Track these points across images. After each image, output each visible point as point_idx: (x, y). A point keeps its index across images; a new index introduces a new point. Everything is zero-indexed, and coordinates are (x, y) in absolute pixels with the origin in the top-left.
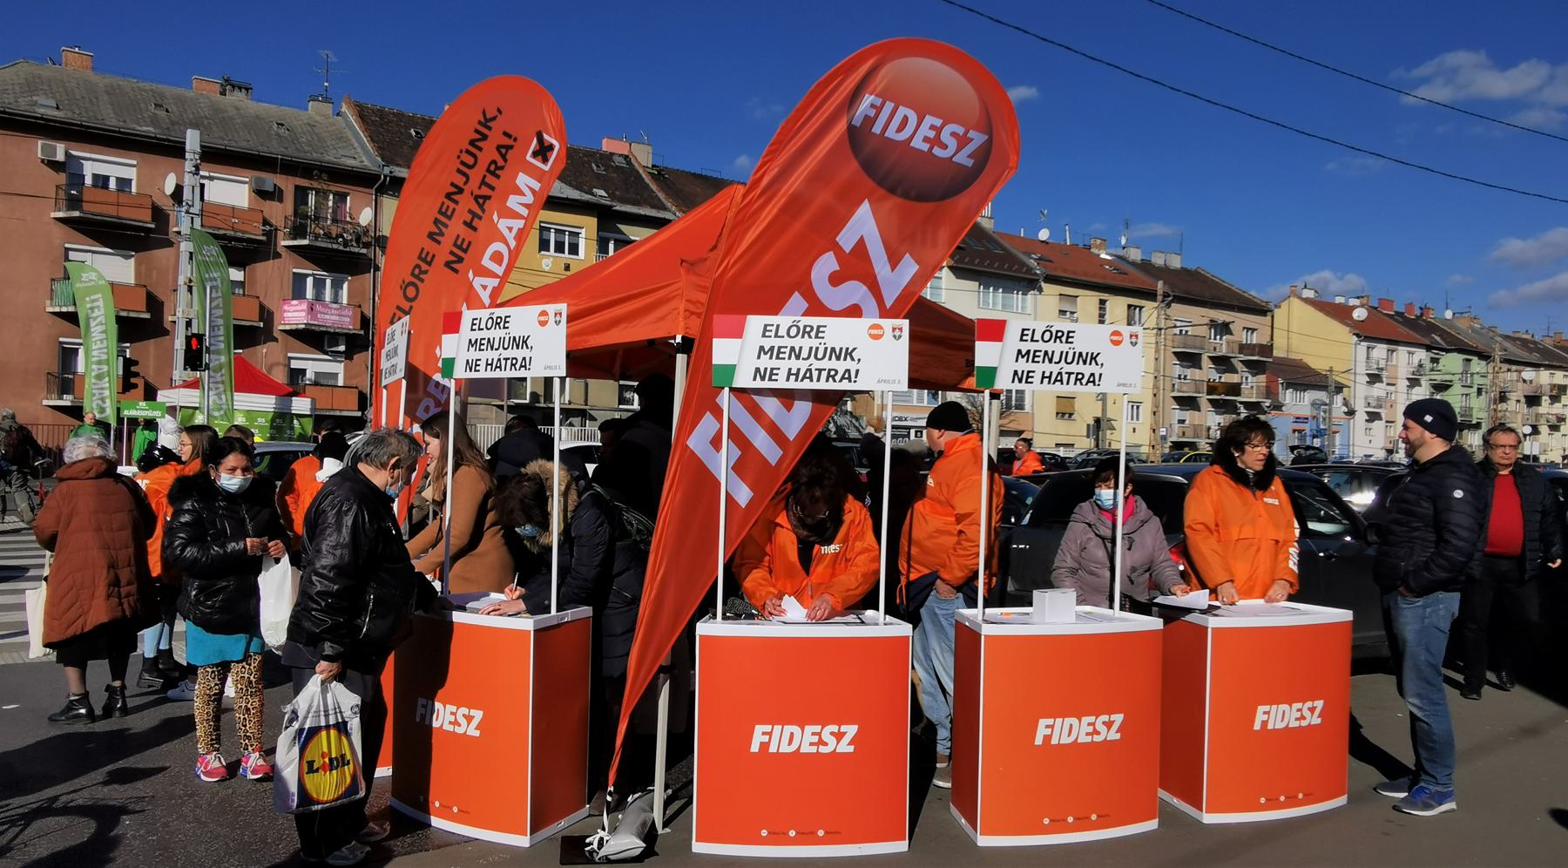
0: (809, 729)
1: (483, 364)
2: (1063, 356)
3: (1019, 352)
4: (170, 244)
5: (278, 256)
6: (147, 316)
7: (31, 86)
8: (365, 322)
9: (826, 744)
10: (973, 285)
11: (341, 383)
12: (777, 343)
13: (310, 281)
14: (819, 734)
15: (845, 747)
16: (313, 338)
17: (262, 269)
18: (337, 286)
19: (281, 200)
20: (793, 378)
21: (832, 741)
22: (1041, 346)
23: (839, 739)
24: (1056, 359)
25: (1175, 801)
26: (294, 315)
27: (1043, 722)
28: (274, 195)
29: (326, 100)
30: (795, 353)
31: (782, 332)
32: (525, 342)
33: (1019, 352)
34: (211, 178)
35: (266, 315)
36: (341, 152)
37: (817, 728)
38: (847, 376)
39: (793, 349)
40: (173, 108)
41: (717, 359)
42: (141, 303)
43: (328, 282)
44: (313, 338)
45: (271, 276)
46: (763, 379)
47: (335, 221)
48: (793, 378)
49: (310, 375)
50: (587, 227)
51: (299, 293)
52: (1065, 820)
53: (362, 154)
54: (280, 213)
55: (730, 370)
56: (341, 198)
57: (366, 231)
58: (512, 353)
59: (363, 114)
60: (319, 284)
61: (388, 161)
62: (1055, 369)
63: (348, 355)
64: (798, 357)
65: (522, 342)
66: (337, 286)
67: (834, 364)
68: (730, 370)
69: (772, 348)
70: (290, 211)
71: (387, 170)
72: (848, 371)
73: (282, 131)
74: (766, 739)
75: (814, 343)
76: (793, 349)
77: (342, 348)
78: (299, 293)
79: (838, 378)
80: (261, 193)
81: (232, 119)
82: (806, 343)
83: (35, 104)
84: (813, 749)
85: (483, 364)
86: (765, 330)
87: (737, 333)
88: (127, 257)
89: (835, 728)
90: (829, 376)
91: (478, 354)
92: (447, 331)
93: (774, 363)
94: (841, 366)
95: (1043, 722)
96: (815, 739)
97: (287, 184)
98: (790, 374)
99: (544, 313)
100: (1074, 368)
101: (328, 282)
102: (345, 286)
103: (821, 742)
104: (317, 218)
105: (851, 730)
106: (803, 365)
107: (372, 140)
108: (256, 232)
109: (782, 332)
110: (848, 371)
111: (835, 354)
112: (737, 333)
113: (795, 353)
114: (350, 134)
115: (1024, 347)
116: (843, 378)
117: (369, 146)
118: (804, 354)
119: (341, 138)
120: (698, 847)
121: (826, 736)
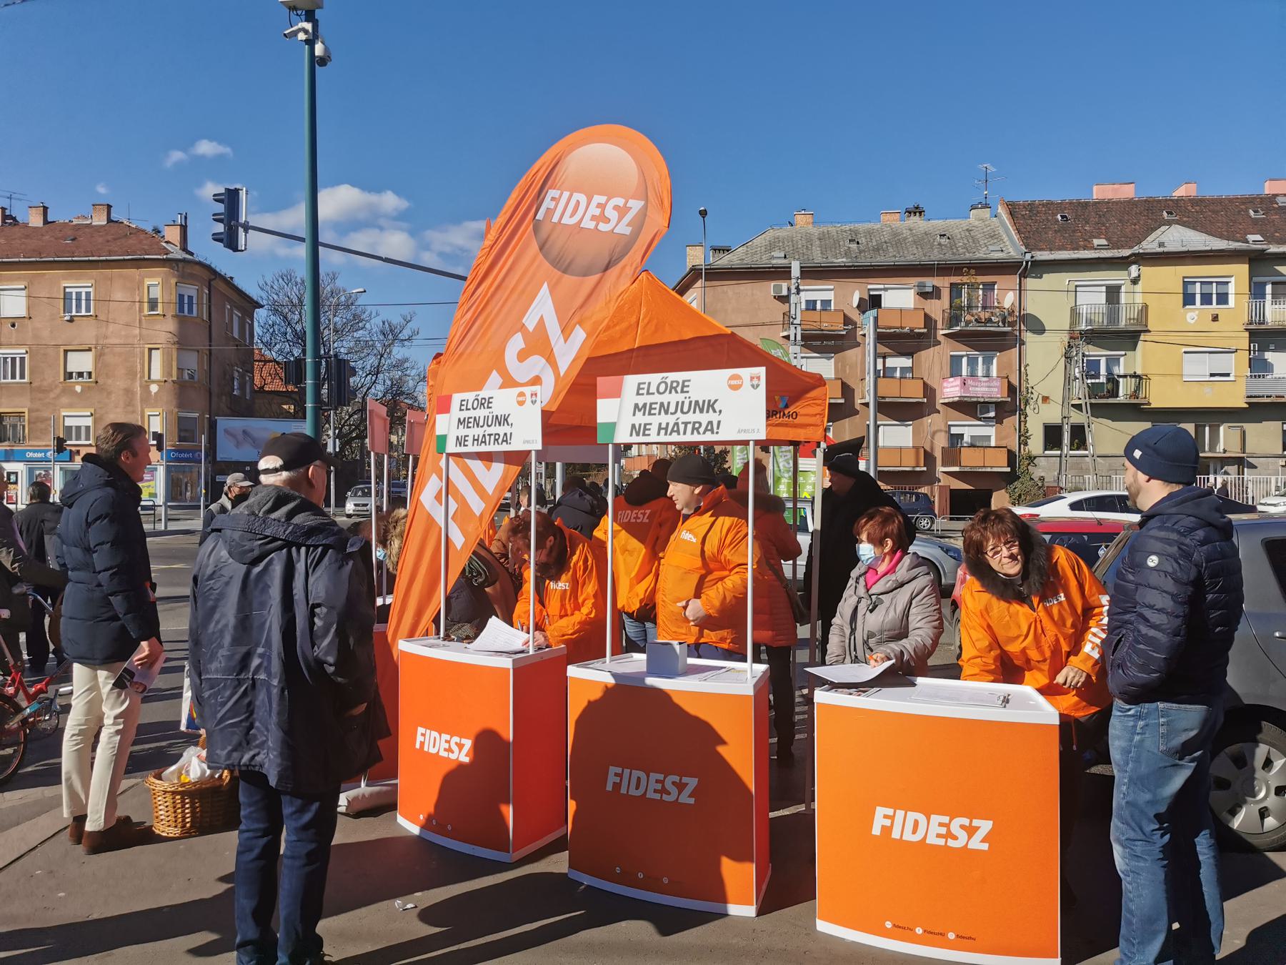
0: (936, 819)
1: (470, 439)
3: (636, 406)
4: (858, 345)
5: (939, 343)
6: (842, 401)
7: (771, 246)
8: (1012, 390)
9: (955, 838)
11: (993, 444)
12: (648, 399)
13: (965, 360)
14: (947, 826)
15: (977, 844)
16: (968, 407)
17: (926, 355)
18: (988, 362)
19: (939, 298)
20: (663, 432)
21: (963, 836)
22: (657, 398)
23: (975, 835)
24: (672, 409)
25: (463, 946)
26: (951, 390)
27: (881, 811)
28: (935, 294)
29: (986, 206)
30: (664, 408)
31: (653, 389)
32: (506, 420)
33: (636, 406)
34: (886, 289)
35: (929, 391)
36: (991, 248)
37: (946, 819)
38: (710, 427)
39: (662, 404)
40: (862, 240)
41: (601, 419)
42: (838, 392)
43: (980, 359)
44: (968, 407)
45: (933, 360)
46: (638, 434)
47: (984, 308)
48: (663, 432)
49: (967, 439)
50: (1237, 276)
51: (955, 372)
53: (1011, 247)
54: (938, 308)
55: (612, 427)
56: (989, 287)
57: (1011, 313)
58: (494, 429)
59: (1013, 209)
60: (972, 362)
61: (1030, 248)
62: (671, 419)
63: (999, 420)
64: (666, 412)
65: (503, 420)
66: (988, 362)
67: (697, 417)
68: (612, 427)
69: (645, 405)
70: (947, 305)
71: (1028, 257)
72: (710, 423)
73: (944, 241)
74: (888, 822)
75: (680, 397)
76: (662, 404)
77: (992, 414)
78: (955, 372)
79: (702, 430)
80: (924, 295)
81: (905, 239)
82: (672, 398)
83: (773, 258)
84: (941, 842)
85: (470, 439)
86: (639, 389)
87: (616, 393)
88: (829, 358)
90: (693, 429)
91: (466, 432)
92: (440, 412)
93: (648, 419)
94: (704, 418)
96: (943, 830)
97: (943, 282)
98: (660, 428)
99: (521, 394)
100: (691, 417)
101: (980, 359)
102: (995, 361)
103: (950, 835)
104: (970, 307)
105: (985, 826)
106: (671, 419)
107: (1019, 232)
108: (919, 325)
109: (653, 389)
111: (699, 407)
112: (616, 393)
113: (664, 408)
114: (1001, 231)
115: (641, 401)
116: (706, 430)
117: (1016, 237)
118: (672, 409)
119: (993, 236)
120: (822, 926)
121: (955, 828)
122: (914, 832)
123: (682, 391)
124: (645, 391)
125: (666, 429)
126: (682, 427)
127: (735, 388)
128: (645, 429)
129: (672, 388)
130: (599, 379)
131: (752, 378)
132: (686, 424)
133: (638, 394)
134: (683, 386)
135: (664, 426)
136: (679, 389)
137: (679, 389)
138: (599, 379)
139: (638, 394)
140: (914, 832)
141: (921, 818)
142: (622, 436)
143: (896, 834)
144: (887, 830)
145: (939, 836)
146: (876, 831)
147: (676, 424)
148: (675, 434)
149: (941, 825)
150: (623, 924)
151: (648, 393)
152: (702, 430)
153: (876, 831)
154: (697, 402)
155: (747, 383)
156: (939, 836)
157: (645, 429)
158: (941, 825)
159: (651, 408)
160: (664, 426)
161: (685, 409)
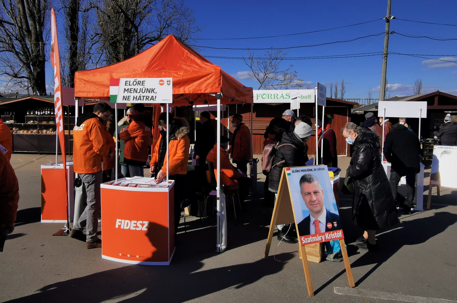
2: (141, 90)
3: (125, 89)
9: (138, 227)
10: (46, 63)
14: (136, 224)
20: (135, 99)
21: (140, 226)
22: (133, 87)
24: (138, 91)
27: (118, 220)
33: (125, 89)
37: (136, 222)
38: (152, 98)
39: (135, 89)
46: (126, 100)
48: (135, 99)
52: (127, 256)
55: (115, 97)
62: (138, 95)
64: (136, 92)
68: (115, 97)
69: (128, 89)
72: (153, 96)
74: (120, 224)
76: (135, 89)
79: (149, 99)
82: (139, 87)
84: (134, 229)
86: (126, 83)
89: (141, 222)
90: (146, 98)
94: (150, 95)
95: (118, 220)
96: (135, 225)
98: (134, 98)
100: (145, 94)
103: (137, 227)
106: (138, 95)
110: (153, 96)
111: (148, 91)
115: (127, 87)
116: (151, 99)
120: (104, 257)
122: (127, 226)
123: (142, 85)
124: (128, 84)
125: (136, 98)
126: (142, 98)
127: (162, 84)
128: (127, 98)
129: (139, 83)
130: (426, 102)
131: (168, 82)
132: (144, 97)
133: (125, 85)
134: (143, 83)
135: (135, 97)
136: (141, 84)
137: (141, 84)
138: (426, 102)
139: (125, 85)
140: (127, 226)
141: (129, 222)
142: (120, 100)
143: (122, 227)
144: (120, 226)
145: (134, 227)
146: (117, 227)
147: (140, 96)
148: (152, 100)
149: (134, 223)
150: (431, 238)
151: (129, 85)
152: (149, 99)
153: (117, 227)
154: (148, 89)
155: (166, 83)
156: (134, 227)
157: (128, 98)
158: (134, 223)
159: (130, 91)
160: (135, 97)
161: (143, 91)
